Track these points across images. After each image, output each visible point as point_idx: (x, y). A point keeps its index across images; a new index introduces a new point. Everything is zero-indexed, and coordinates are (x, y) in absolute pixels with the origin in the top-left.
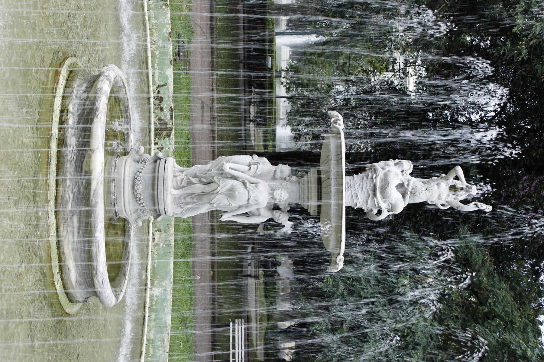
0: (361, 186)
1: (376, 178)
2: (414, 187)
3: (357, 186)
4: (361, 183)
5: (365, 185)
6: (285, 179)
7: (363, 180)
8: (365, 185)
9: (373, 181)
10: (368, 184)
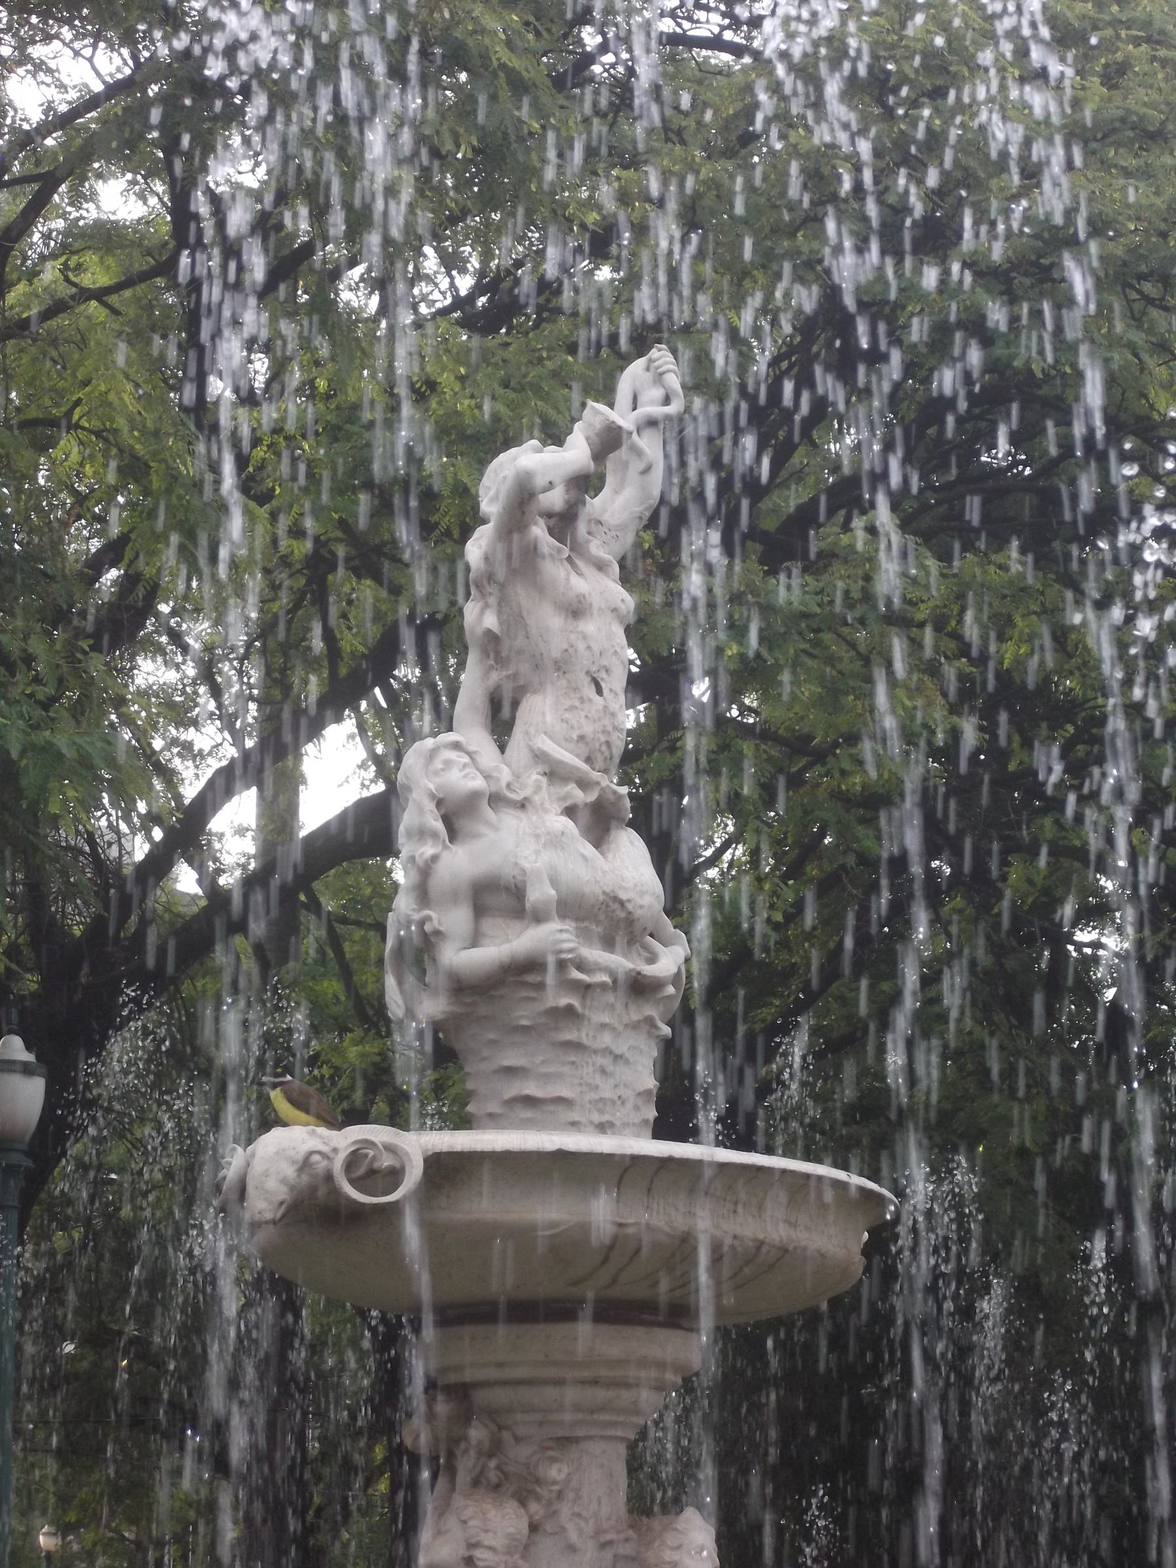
0: (606, 1062)
1: (581, 966)
2: (584, 749)
3: (607, 1092)
4: (600, 1060)
5: (606, 1039)
6: (534, 1528)
7: (578, 1047)
8: (606, 1039)
9: (603, 986)
10: (606, 1018)
